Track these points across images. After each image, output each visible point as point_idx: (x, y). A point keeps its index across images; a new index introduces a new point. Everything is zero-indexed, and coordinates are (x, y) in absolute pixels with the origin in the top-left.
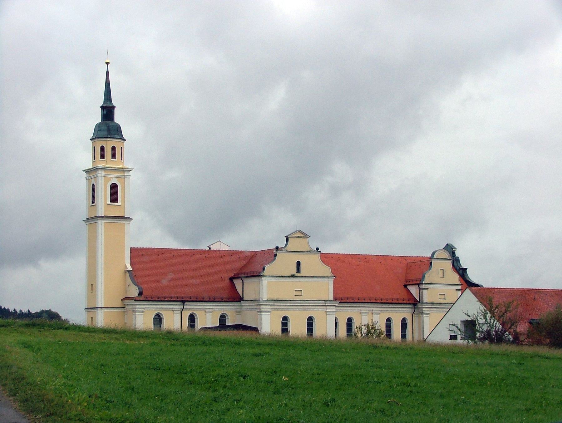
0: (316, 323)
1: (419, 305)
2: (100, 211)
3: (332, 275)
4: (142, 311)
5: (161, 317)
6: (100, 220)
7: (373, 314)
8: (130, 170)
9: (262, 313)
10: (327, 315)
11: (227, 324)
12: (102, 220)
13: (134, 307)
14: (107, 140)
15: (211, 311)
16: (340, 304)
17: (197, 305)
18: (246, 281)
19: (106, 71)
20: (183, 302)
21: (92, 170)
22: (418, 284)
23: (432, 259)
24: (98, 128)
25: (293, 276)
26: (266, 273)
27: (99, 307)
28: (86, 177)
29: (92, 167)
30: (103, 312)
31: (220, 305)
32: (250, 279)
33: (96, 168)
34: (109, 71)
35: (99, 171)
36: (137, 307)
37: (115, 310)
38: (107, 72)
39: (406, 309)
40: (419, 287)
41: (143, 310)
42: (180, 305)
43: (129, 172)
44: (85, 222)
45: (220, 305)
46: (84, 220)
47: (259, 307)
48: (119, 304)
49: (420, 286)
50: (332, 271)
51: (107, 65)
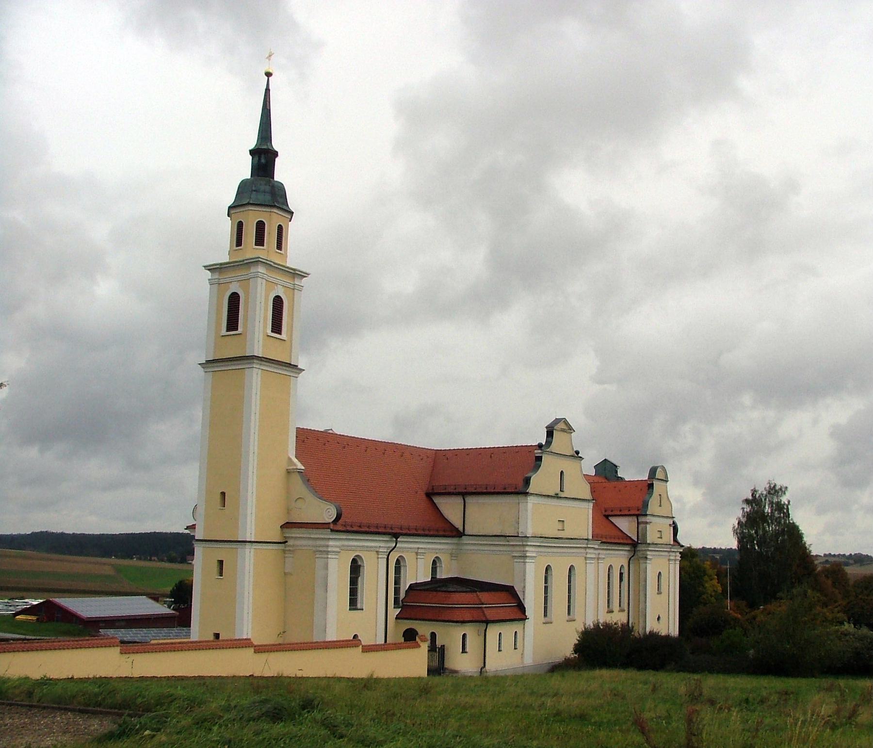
0: (407, 568)
1: (640, 548)
2: (256, 347)
3: (588, 496)
4: (336, 552)
5: (360, 563)
6: (258, 363)
7: (378, 554)
8: (305, 275)
9: (527, 561)
10: (417, 558)
11: (438, 577)
12: (261, 364)
13: (319, 543)
14: (272, 210)
15: (423, 553)
16: (602, 544)
17: (376, 540)
18: (470, 500)
19: (265, 87)
20: (396, 536)
21: (241, 263)
22: (637, 516)
23: (654, 479)
24: (243, 187)
25: (556, 496)
26: (531, 490)
27: (248, 540)
28: (209, 280)
29: (227, 260)
30: (252, 550)
31: (372, 540)
32: (491, 498)
33: (257, 260)
34: (270, 88)
35: (259, 267)
36: (331, 543)
37: (270, 546)
38: (267, 90)
39: (621, 552)
40: (638, 520)
41: (338, 549)
42: (387, 541)
43: (302, 279)
44: (203, 367)
45: (372, 540)
46: (199, 364)
47: (522, 549)
48: (275, 534)
49: (639, 519)
50: (593, 491)
51: (267, 78)
